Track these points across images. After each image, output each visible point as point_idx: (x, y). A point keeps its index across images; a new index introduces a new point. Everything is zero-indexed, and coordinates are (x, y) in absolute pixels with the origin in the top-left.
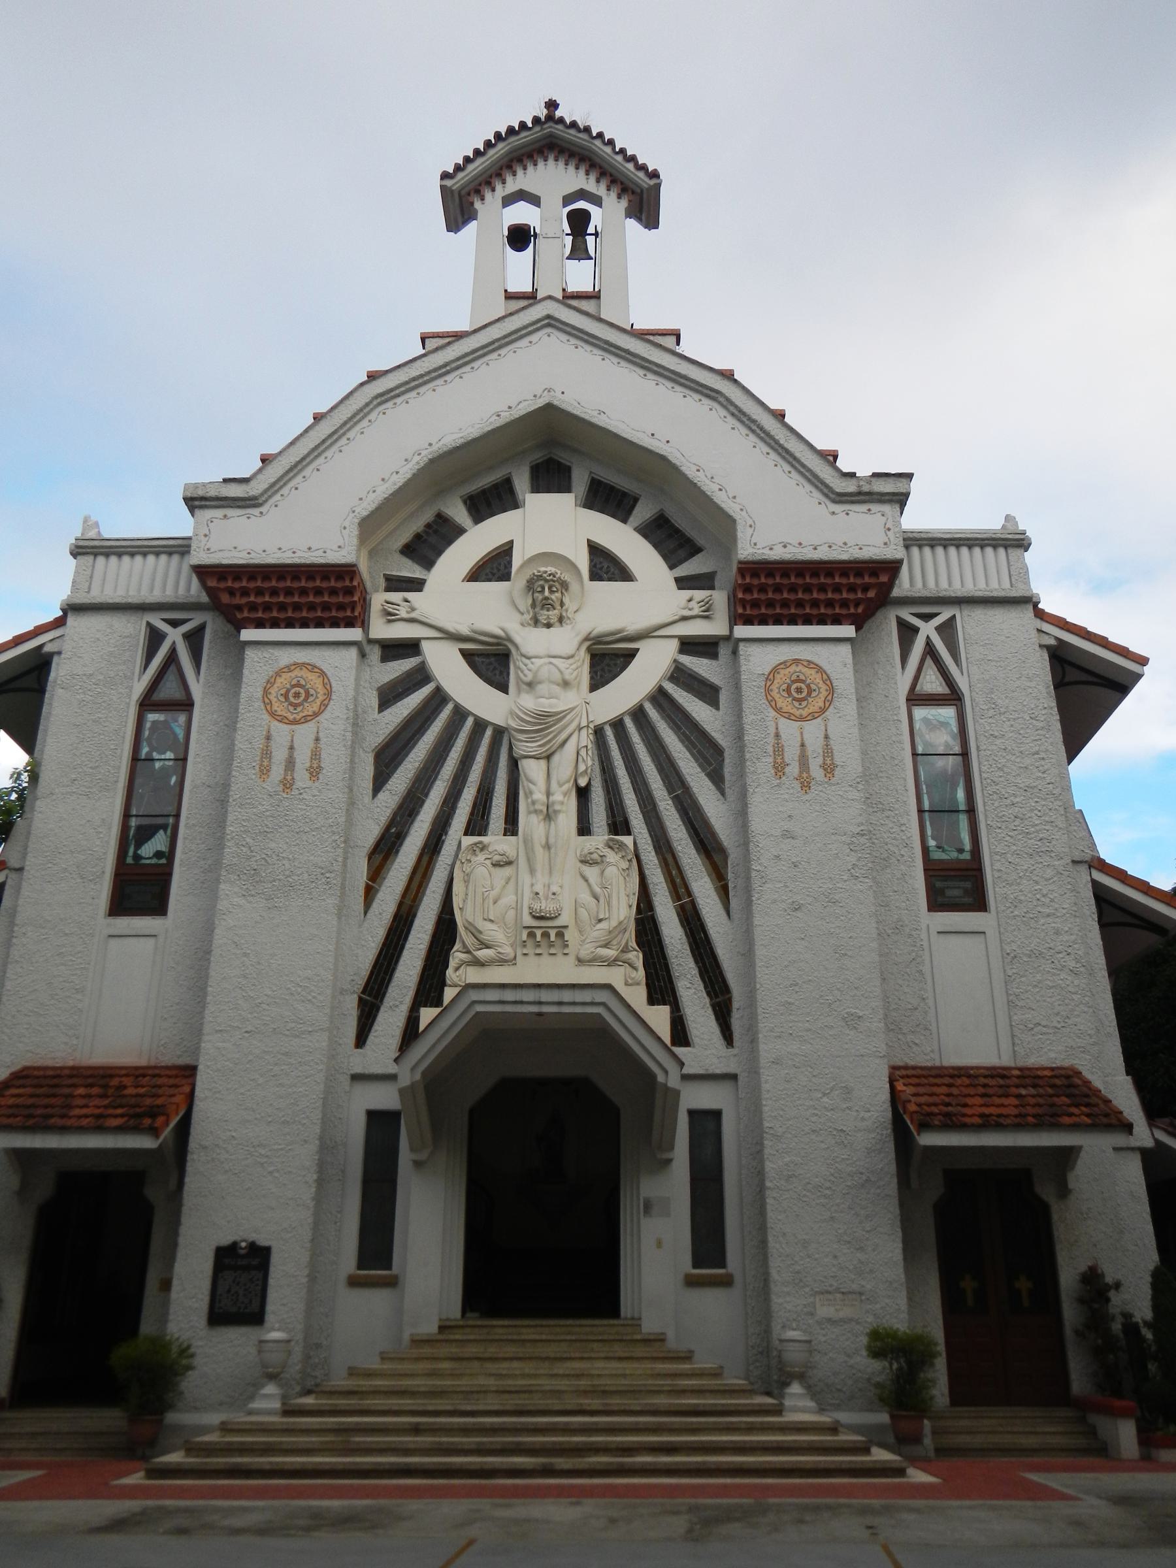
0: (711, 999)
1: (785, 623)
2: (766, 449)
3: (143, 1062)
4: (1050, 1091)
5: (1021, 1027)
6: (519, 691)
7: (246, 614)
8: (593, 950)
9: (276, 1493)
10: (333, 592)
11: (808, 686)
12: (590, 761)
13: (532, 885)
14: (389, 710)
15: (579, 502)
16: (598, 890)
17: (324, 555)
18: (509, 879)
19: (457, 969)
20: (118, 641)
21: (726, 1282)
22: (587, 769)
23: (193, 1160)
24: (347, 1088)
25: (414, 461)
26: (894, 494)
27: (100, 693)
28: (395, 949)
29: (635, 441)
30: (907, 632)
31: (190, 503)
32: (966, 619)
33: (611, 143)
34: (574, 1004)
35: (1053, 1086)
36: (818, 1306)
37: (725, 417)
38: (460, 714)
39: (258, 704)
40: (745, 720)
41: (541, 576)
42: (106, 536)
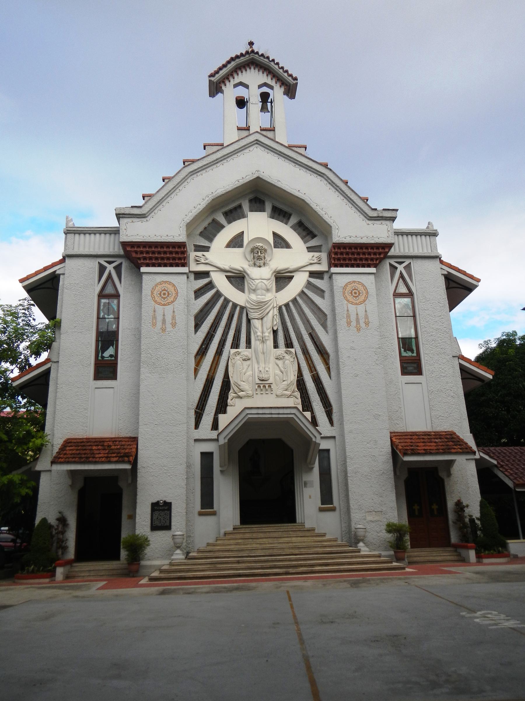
0: (325, 409)
1: (350, 267)
2: (342, 198)
3: (113, 436)
4: (446, 440)
5: (434, 417)
6: (249, 292)
7: (142, 261)
8: (282, 392)
9: (210, 583)
10: (177, 253)
11: (359, 291)
12: (278, 320)
13: (258, 368)
14: (199, 299)
15: (268, 216)
16: (282, 369)
17: (173, 238)
18: (249, 366)
19: (232, 400)
20: (87, 270)
21: (333, 509)
22: (277, 323)
23: (140, 472)
24: (193, 445)
25: (206, 200)
26: (391, 217)
27: (82, 291)
28: (207, 392)
29: (292, 193)
30: (393, 268)
31: (118, 216)
32: (414, 264)
33: (278, 64)
34: (284, 414)
35: (446, 438)
36: (367, 516)
37: (326, 184)
38: (227, 301)
39: (150, 298)
40: (336, 304)
41: (257, 247)
42: (76, 226)
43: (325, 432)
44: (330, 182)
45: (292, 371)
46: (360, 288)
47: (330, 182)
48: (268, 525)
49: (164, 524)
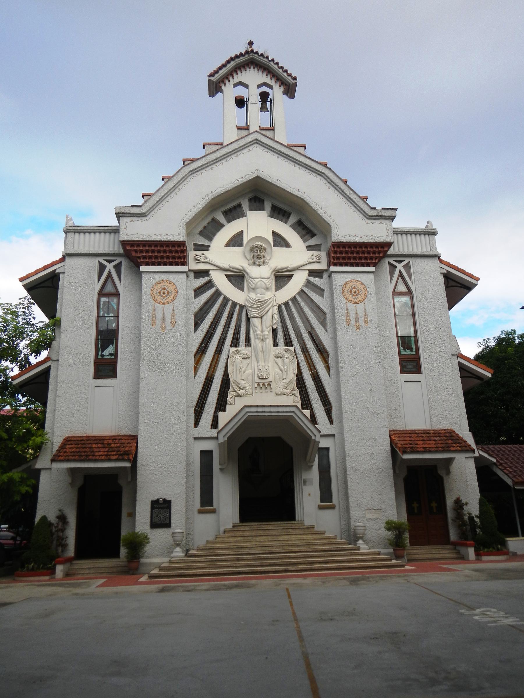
0: (324, 407)
1: (349, 266)
2: (342, 197)
3: (113, 434)
4: (445, 438)
5: (433, 415)
6: (249, 291)
7: (142, 260)
8: (281, 390)
9: (209, 581)
10: (176, 252)
11: (358, 290)
12: (277, 319)
13: (258, 366)
14: (199, 298)
15: (268, 215)
16: (282, 367)
17: (173, 237)
18: (248, 364)
19: (231, 398)
20: (87, 269)
21: (333, 507)
22: (276, 322)
23: (140, 470)
24: (193, 443)
25: (206, 199)
26: (390, 216)
27: (82, 290)
28: (207, 390)
29: (292, 192)
30: (393, 267)
31: (118, 215)
32: (414, 263)
33: (277, 63)
34: (283, 412)
35: (446, 436)
36: (366, 514)
37: (326, 183)
38: (226, 300)
39: (149, 296)
40: (335, 303)
41: (257, 246)
42: (76, 225)
43: (324, 430)
44: (330, 181)
45: (291, 370)
46: (360, 286)
47: (330, 181)
48: (268, 523)
49: (164, 522)
